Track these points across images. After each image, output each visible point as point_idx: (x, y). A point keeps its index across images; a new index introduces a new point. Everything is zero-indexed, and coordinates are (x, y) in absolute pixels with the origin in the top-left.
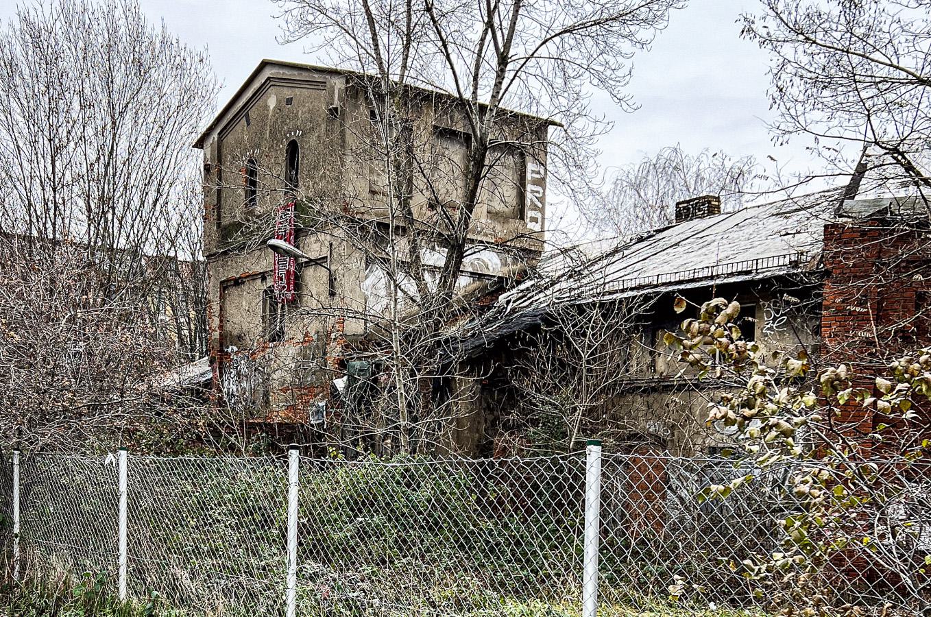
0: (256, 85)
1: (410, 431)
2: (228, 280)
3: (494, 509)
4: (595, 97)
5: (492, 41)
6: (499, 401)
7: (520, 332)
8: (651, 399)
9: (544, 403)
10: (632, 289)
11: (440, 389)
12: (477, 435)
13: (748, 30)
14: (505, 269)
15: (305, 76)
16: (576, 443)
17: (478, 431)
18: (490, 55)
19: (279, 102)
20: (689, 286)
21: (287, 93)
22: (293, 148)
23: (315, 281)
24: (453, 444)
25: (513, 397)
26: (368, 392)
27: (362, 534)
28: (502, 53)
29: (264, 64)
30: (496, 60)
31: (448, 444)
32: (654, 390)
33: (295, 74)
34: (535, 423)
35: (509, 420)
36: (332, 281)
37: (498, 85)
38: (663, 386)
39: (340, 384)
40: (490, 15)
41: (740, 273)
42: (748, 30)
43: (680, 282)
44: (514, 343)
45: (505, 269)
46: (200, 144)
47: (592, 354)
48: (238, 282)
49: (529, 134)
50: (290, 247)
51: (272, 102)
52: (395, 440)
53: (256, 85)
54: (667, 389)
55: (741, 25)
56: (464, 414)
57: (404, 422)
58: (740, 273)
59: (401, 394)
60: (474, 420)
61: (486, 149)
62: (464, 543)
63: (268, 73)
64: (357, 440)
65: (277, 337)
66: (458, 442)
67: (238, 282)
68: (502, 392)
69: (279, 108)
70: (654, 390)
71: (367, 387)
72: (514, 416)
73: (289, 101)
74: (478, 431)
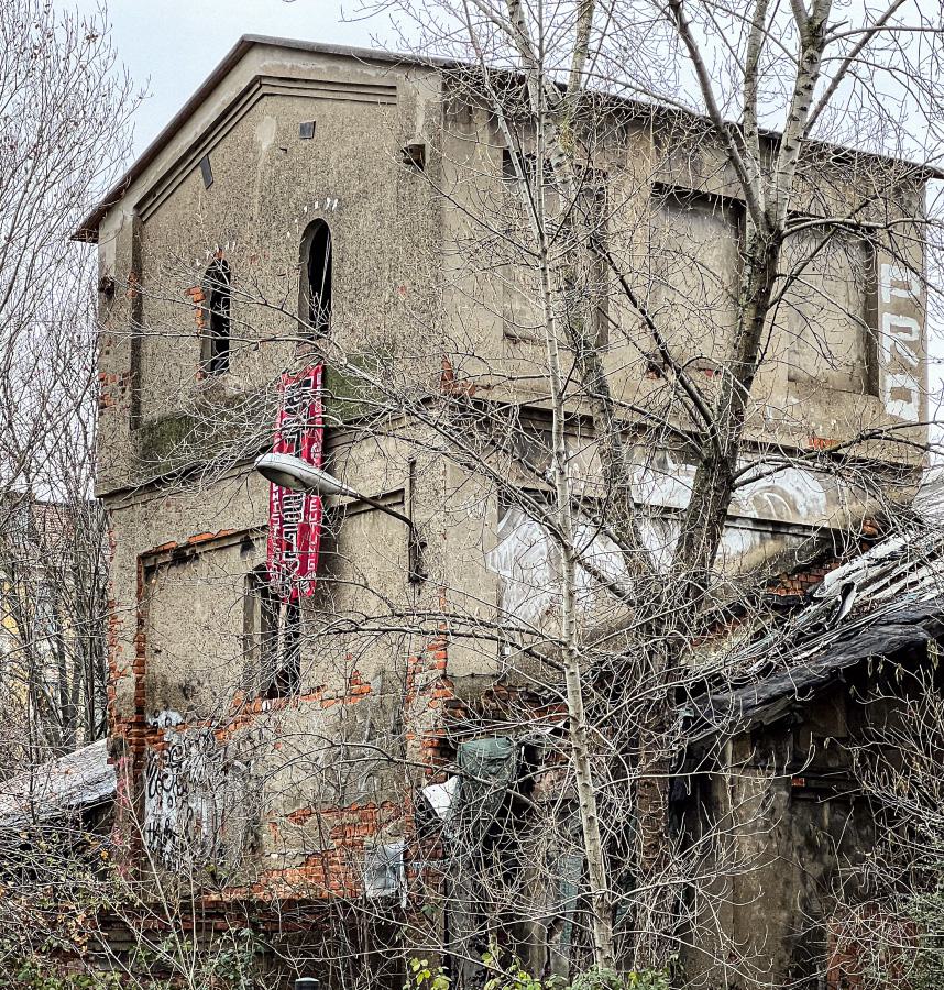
6: (834, 829)
11: (691, 804)
12: (784, 915)
15: (344, 72)
17: (785, 905)
21: (304, 112)
22: (318, 238)
23: (372, 548)
28: (810, 22)
29: (246, 47)
39: (441, 797)
61: (779, 238)
65: (282, 685)
66: (736, 935)
72: (870, 867)
73: (308, 130)
74: (785, 905)
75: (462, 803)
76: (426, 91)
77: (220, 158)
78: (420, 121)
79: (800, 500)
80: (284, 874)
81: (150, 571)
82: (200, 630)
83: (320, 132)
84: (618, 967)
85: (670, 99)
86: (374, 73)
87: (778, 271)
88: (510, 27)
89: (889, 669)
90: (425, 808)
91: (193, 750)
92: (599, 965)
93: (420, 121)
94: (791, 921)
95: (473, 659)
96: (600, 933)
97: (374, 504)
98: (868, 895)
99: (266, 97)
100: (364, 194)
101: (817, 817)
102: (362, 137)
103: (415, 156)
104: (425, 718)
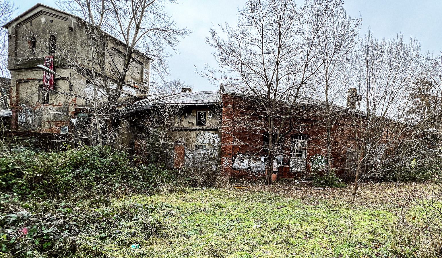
0: (35, 12)
1: (103, 138)
2: (21, 80)
3: (136, 164)
4: (168, 48)
5: (134, 22)
6: (137, 130)
7: (143, 110)
8: (181, 132)
9: (153, 131)
10: (176, 104)
11: (116, 124)
12: (129, 140)
13: (207, 41)
14: (137, 95)
15: (58, 14)
16: (163, 143)
17: (129, 139)
18: (134, 25)
19: (46, 20)
20: (191, 104)
21: (51, 18)
22: (53, 37)
23: (63, 86)
24: (120, 142)
25: (142, 129)
26: (85, 125)
27: (78, 177)
28: (137, 25)
29: (39, 6)
30: (135, 26)
31: (119, 142)
32: (182, 130)
33: (54, 12)
34: (149, 137)
35: (141, 136)
36: (71, 86)
37: (135, 37)
38: (184, 130)
39: (74, 121)
40: (134, 17)
41: (203, 103)
42: (207, 41)
43: (188, 103)
44: (142, 113)
45: (137, 95)
46: (6, 26)
47: (168, 117)
48: (27, 81)
49: (144, 60)
50: (52, 71)
51: (43, 20)
52: (97, 141)
53: (35, 12)
54: (185, 130)
55: (206, 40)
56: (124, 132)
57: (100, 134)
58: (203, 103)
59: (98, 124)
60: (128, 134)
61: (132, 53)
62: (125, 177)
63: (40, 9)
64: (78, 140)
65: (46, 102)
66: (122, 142)
67: (27, 81)
68: (137, 127)
69: (46, 23)
70: (182, 130)
71: (84, 121)
72: (142, 134)
73: (51, 21)
74: (129, 139)
75: (77, 122)
76: (73, 21)
77: (33, 21)
78: (72, 24)
79: (132, 92)
80: (46, 128)
81: (19, 83)
82: (30, 92)
83: (53, 22)
84: (103, 145)
85: (129, 34)
86: (64, 16)
87: (84, 104)
88: (153, 38)
89: (145, 111)
90: (71, 123)
91: (28, 110)
92: (99, 144)
93: (72, 24)
94: (130, 141)
95: (81, 102)
96: (100, 140)
97: (64, 79)
98: (142, 138)
99: (43, 15)
100: (62, 33)
101: (134, 129)
102: (65, 25)
103: (71, 29)
104: (72, 110)
